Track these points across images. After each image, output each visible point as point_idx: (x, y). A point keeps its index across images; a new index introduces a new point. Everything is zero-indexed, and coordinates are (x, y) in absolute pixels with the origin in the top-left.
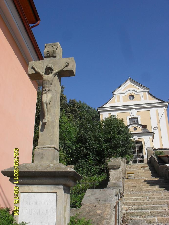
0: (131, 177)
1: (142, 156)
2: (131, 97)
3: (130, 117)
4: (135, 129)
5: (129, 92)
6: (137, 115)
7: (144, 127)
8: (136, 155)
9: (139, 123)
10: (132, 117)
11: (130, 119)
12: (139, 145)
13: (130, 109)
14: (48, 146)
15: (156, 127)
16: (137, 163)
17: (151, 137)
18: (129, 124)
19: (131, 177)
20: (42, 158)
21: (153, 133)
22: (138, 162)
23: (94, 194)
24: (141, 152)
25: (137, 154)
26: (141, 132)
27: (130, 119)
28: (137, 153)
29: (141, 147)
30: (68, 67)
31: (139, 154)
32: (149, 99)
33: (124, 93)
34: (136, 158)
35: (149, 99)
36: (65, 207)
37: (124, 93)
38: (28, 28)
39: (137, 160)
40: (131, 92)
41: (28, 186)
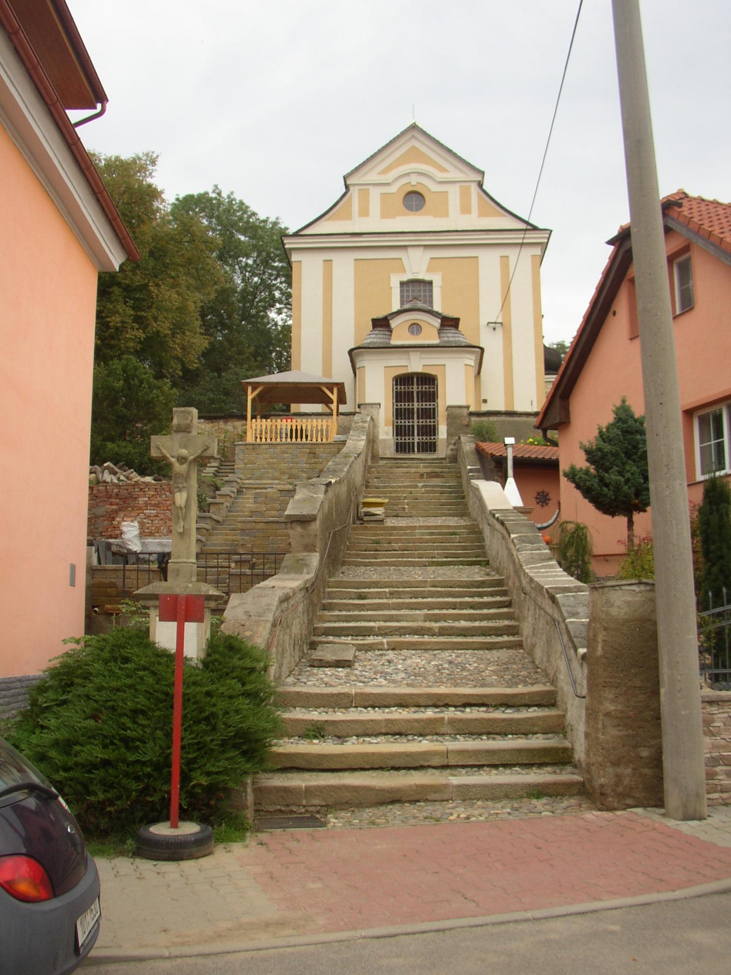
0: (372, 518)
1: (432, 431)
2: (414, 198)
3: (405, 278)
4: (415, 328)
5: (405, 180)
6: (429, 270)
7: (450, 323)
8: (411, 424)
9: (437, 307)
10: (411, 277)
11: (402, 284)
12: (425, 388)
13: (405, 247)
14: (185, 560)
15: (495, 323)
16: (413, 451)
17: (472, 363)
18: (396, 306)
19: (372, 518)
20: (178, 575)
21: (479, 347)
22: (418, 451)
23: (244, 604)
24: (430, 414)
25: (416, 420)
26: (436, 341)
27: (402, 284)
28: (418, 418)
29: (432, 396)
30: (208, 451)
31: (423, 422)
32: (481, 214)
33: (388, 184)
34: (413, 435)
35: (481, 214)
36: (206, 631)
37: (388, 184)
38: (67, 128)
39: (416, 440)
40: (414, 180)
41: (441, 772)
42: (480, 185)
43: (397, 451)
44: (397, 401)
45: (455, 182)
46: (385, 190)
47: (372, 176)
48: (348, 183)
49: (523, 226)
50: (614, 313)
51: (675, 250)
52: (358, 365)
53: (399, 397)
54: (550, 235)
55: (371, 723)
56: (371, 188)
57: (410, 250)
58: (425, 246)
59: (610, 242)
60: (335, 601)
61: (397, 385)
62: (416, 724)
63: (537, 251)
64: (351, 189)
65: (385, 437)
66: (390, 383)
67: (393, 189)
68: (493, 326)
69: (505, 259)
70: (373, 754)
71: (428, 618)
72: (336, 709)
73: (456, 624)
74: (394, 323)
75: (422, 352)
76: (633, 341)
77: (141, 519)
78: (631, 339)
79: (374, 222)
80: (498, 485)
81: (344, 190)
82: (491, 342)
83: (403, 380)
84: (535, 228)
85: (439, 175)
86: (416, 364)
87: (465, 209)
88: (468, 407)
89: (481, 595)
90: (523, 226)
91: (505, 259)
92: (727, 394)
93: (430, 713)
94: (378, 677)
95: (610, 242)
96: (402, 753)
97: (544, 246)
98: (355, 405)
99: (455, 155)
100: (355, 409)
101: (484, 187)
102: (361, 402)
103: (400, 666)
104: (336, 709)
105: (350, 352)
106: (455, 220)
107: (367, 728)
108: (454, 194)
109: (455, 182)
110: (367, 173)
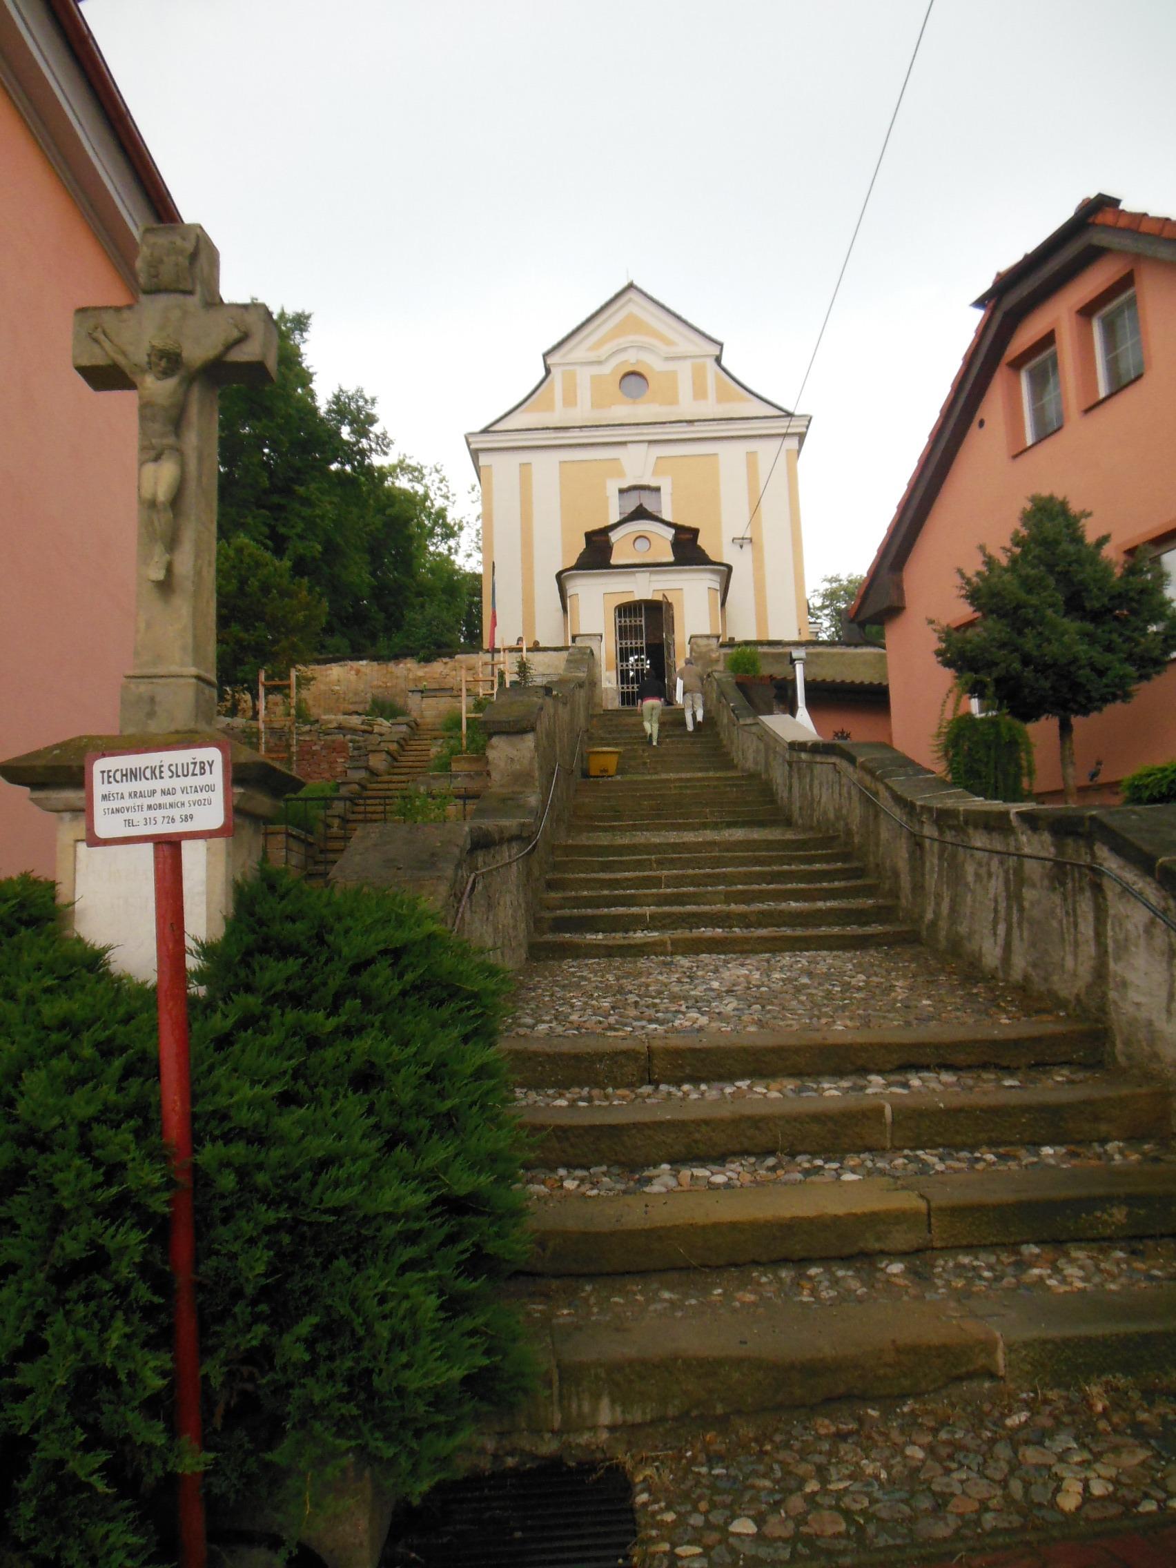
3: (625, 485)
18: (614, 518)
33: (599, 363)
42: (718, 360)
43: (623, 703)
44: (621, 639)
45: (685, 358)
46: (596, 370)
47: (579, 352)
48: (549, 362)
49: (777, 413)
50: (981, 423)
51: (1101, 290)
52: (570, 592)
53: (623, 632)
54: (801, 443)
55: (704, 1129)
56: (578, 369)
57: (629, 446)
58: (650, 442)
59: (980, 303)
60: (567, 876)
61: (620, 616)
62: (816, 1128)
63: (793, 443)
64: (553, 369)
65: (609, 685)
66: (612, 615)
67: (607, 369)
68: (741, 542)
69: (751, 458)
70: (734, 1226)
71: (729, 898)
72: (610, 1090)
73: (783, 906)
74: (614, 536)
75: (651, 572)
76: (1019, 459)
77: (1057, 1408)
78: (1015, 456)
79: (582, 412)
80: (788, 716)
81: (543, 373)
82: (740, 561)
83: (626, 610)
84: (789, 415)
85: (664, 350)
86: (643, 588)
87: (699, 392)
88: (718, 637)
89: (810, 860)
90: (777, 413)
91: (751, 458)
92: (1170, 528)
93: (832, 1091)
94: (683, 1008)
95: (980, 303)
96: (811, 1221)
97: (802, 437)
98: (566, 636)
99: (685, 322)
100: (566, 640)
101: (724, 362)
102: (576, 633)
103: (715, 985)
104: (610, 1090)
105: (559, 576)
106: (687, 407)
107: (696, 1142)
108: (684, 372)
109: (685, 358)
110: (572, 349)
